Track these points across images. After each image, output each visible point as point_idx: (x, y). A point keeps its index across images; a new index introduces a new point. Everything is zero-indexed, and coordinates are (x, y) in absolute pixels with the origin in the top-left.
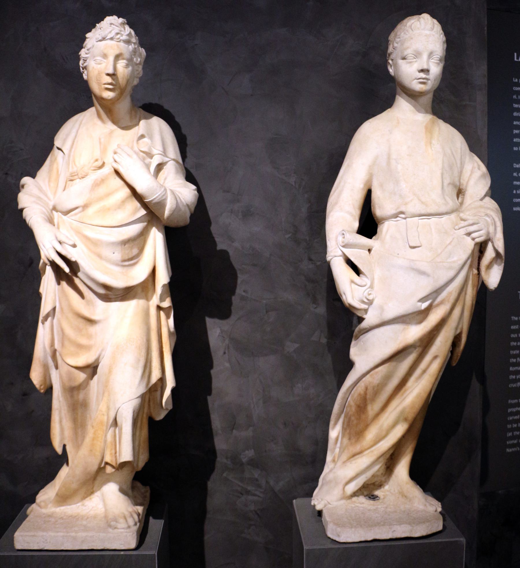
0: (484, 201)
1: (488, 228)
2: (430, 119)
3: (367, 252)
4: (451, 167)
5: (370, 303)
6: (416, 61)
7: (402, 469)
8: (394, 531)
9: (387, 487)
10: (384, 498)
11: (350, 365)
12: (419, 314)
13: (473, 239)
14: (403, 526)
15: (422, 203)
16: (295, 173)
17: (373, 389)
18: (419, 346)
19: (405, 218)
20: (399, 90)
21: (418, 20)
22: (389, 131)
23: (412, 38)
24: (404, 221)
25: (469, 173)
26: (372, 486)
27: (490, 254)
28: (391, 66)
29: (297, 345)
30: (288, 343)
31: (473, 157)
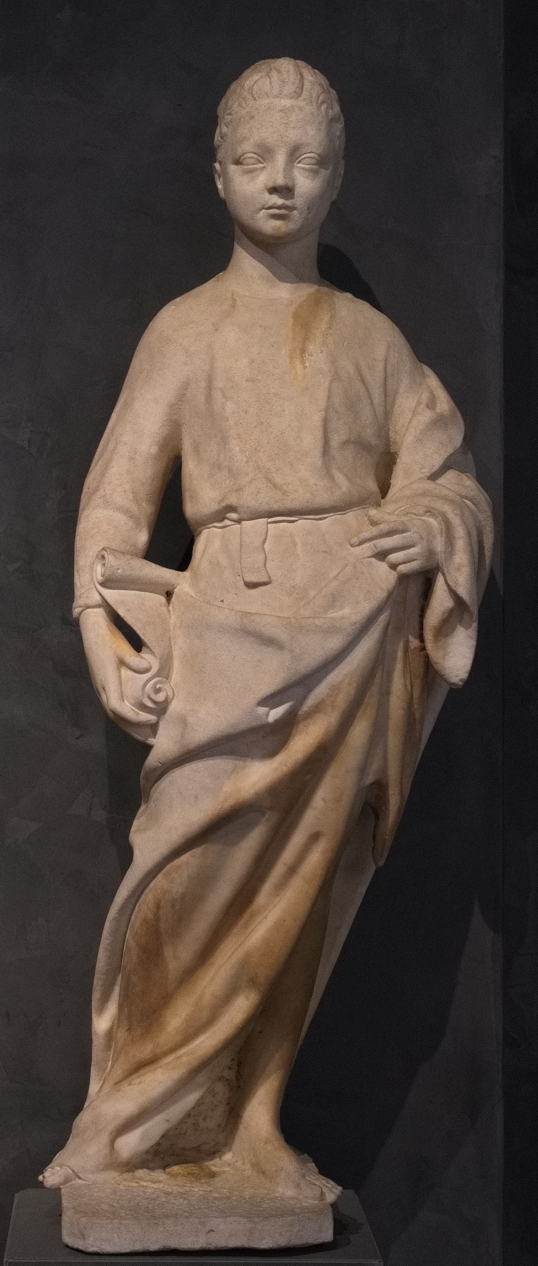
0: (441, 481)
1: (430, 542)
3: (163, 599)
4: (352, 406)
5: (161, 709)
7: (260, 1113)
8: (212, 1231)
9: (228, 1157)
11: (126, 855)
13: (393, 566)
15: (275, 486)
17: (173, 906)
19: (239, 521)
20: (238, 232)
21: (268, 75)
23: (252, 117)
27: (440, 601)
28: (219, 176)
31: (424, 376)
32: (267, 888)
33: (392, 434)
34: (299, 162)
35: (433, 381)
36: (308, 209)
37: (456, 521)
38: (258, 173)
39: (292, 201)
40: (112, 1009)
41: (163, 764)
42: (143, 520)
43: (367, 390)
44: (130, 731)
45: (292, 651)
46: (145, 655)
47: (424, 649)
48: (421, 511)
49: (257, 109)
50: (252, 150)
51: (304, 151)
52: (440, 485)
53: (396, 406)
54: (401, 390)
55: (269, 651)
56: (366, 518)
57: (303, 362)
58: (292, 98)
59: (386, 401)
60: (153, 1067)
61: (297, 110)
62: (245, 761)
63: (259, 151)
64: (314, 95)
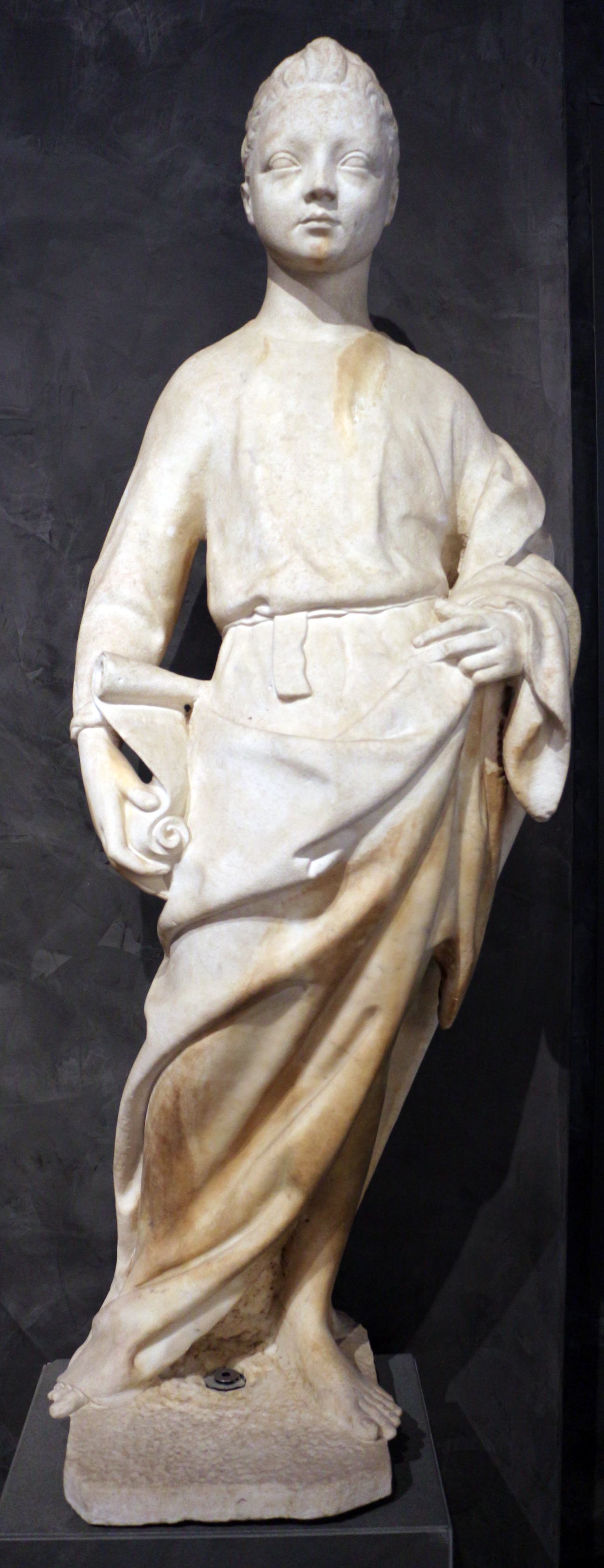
0: (522, 566)
1: (514, 641)
2: (359, 340)
3: (180, 715)
4: (412, 471)
5: (174, 856)
6: (298, 172)
7: (307, 1306)
8: (243, 1500)
9: (271, 1350)
10: (254, 1385)
12: (309, 889)
13: (469, 673)
14: (266, 1486)
15: (317, 570)
16: (51, 509)
17: (195, 1096)
18: (315, 981)
20: (271, 264)
21: (303, 57)
22: (241, 375)
23: (284, 108)
24: (270, 623)
25: (479, 489)
26: (233, 1346)
27: (526, 716)
28: (248, 199)
29: (62, 959)
30: (40, 954)
32: (310, 1071)
33: (460, 512)
34: (343, 164)
35: (506, 450)
36: (356, 224)
37: (545, 616)
40: (135, 1189)
41: (179, 924)
44: (137, 882)
45: (338, 785)
46: (155, 787)
47: (503, 774)
48: (502, 602)
49: (290, 97)
50: (283, 148)
51: (349, 148)
52: (521, 571)
54: (470, 458)
55: (309, 784)
56: (433, 612)
57: (352, 416)
59: (452, 470)
60: (179, 1270)
62: (280, 923)
63: (292, 149)
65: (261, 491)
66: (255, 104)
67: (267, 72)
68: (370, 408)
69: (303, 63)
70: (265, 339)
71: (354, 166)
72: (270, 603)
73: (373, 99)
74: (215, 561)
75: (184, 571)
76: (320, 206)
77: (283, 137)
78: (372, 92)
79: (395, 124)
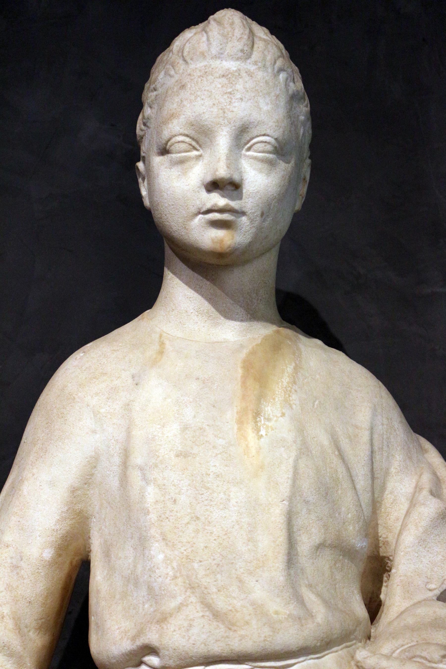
2: (266, 339)
6: (199, 157)
15: (217, 615)
20: (168, 252)
21: (204, 30)
22: (133, 377)
23: (183, 87)
28: (143, 179)
31: (423, 451)
33: (381, 531)
34: (249, 149)
36: (262, 214)
38: (193, 162)
39: (238, 202)
42: (28, 659)
43: (348, 469)
49: (190, 75)
50: (182, 131)
51: (255, 133)
53: (386, 493)
54: (393, 470)
58: (238, 59)
61: (244, 74)
63: (192, 133)
64: (269, 58)
65: (153, 517)
66: (153, 77)
67: (166, 43)
68: (278, 419)
69: (205, 38)
70: (161, 336)
71: (263, 152)
72: (161, 654)
73: (282, 76)
74: (98, 592)
75: (63, 598)
76: (223, 196)
77: (182, 119)
78: (281, 70)
79: (307, 101)
